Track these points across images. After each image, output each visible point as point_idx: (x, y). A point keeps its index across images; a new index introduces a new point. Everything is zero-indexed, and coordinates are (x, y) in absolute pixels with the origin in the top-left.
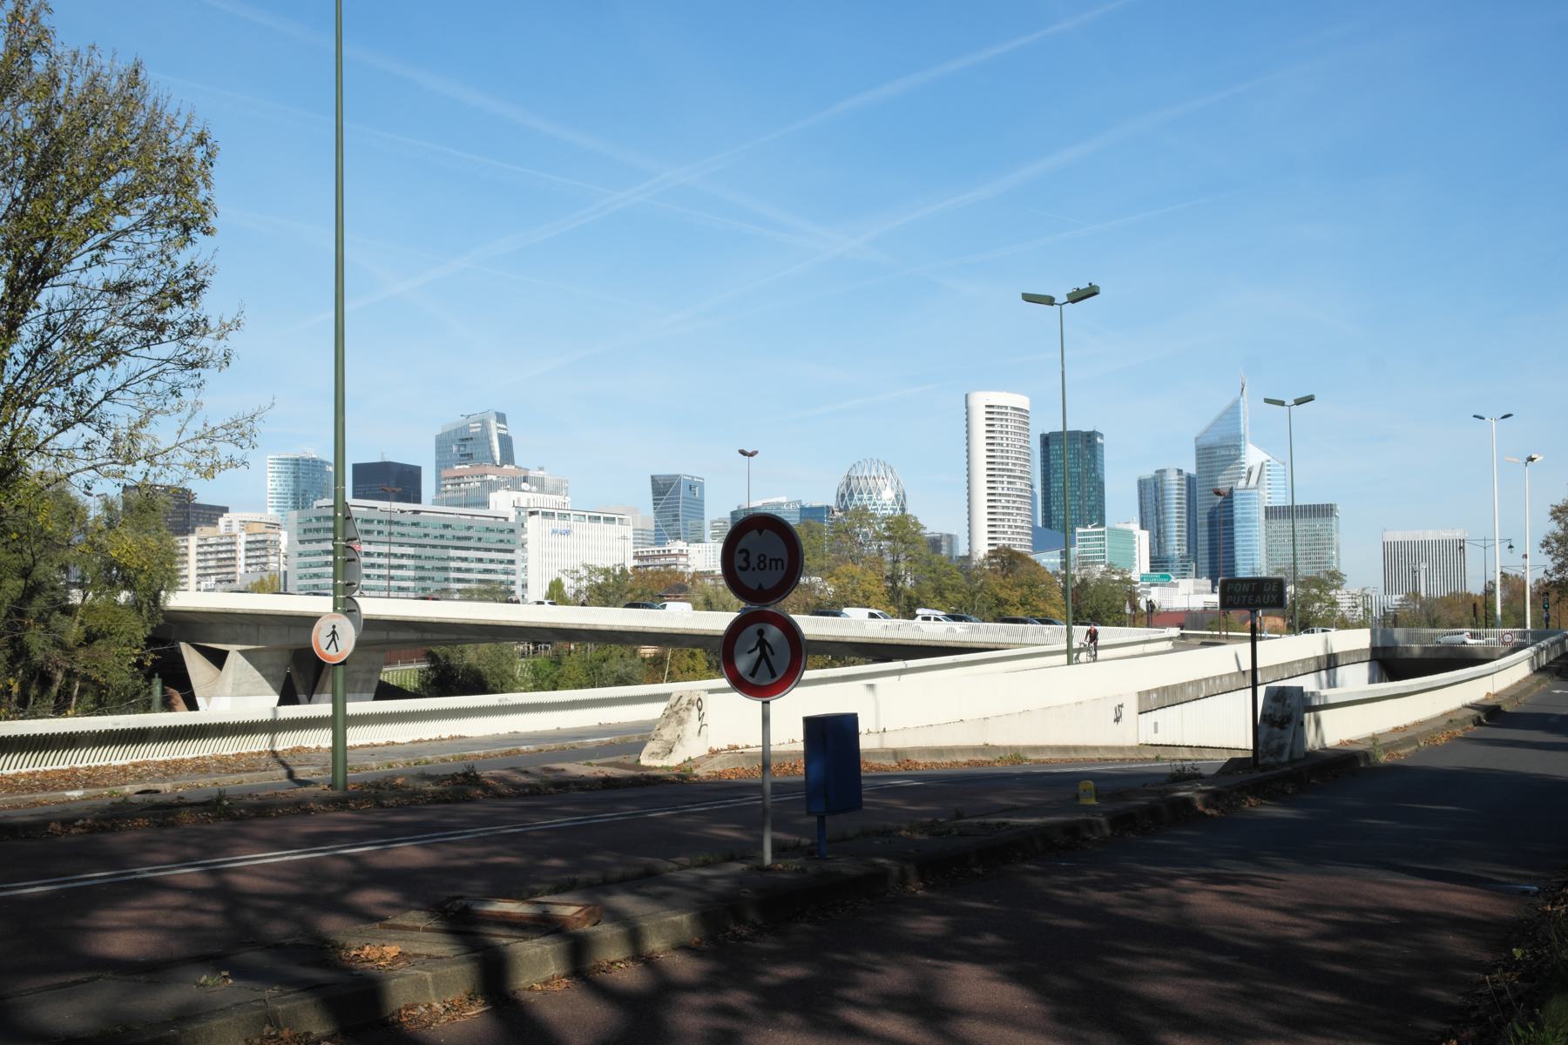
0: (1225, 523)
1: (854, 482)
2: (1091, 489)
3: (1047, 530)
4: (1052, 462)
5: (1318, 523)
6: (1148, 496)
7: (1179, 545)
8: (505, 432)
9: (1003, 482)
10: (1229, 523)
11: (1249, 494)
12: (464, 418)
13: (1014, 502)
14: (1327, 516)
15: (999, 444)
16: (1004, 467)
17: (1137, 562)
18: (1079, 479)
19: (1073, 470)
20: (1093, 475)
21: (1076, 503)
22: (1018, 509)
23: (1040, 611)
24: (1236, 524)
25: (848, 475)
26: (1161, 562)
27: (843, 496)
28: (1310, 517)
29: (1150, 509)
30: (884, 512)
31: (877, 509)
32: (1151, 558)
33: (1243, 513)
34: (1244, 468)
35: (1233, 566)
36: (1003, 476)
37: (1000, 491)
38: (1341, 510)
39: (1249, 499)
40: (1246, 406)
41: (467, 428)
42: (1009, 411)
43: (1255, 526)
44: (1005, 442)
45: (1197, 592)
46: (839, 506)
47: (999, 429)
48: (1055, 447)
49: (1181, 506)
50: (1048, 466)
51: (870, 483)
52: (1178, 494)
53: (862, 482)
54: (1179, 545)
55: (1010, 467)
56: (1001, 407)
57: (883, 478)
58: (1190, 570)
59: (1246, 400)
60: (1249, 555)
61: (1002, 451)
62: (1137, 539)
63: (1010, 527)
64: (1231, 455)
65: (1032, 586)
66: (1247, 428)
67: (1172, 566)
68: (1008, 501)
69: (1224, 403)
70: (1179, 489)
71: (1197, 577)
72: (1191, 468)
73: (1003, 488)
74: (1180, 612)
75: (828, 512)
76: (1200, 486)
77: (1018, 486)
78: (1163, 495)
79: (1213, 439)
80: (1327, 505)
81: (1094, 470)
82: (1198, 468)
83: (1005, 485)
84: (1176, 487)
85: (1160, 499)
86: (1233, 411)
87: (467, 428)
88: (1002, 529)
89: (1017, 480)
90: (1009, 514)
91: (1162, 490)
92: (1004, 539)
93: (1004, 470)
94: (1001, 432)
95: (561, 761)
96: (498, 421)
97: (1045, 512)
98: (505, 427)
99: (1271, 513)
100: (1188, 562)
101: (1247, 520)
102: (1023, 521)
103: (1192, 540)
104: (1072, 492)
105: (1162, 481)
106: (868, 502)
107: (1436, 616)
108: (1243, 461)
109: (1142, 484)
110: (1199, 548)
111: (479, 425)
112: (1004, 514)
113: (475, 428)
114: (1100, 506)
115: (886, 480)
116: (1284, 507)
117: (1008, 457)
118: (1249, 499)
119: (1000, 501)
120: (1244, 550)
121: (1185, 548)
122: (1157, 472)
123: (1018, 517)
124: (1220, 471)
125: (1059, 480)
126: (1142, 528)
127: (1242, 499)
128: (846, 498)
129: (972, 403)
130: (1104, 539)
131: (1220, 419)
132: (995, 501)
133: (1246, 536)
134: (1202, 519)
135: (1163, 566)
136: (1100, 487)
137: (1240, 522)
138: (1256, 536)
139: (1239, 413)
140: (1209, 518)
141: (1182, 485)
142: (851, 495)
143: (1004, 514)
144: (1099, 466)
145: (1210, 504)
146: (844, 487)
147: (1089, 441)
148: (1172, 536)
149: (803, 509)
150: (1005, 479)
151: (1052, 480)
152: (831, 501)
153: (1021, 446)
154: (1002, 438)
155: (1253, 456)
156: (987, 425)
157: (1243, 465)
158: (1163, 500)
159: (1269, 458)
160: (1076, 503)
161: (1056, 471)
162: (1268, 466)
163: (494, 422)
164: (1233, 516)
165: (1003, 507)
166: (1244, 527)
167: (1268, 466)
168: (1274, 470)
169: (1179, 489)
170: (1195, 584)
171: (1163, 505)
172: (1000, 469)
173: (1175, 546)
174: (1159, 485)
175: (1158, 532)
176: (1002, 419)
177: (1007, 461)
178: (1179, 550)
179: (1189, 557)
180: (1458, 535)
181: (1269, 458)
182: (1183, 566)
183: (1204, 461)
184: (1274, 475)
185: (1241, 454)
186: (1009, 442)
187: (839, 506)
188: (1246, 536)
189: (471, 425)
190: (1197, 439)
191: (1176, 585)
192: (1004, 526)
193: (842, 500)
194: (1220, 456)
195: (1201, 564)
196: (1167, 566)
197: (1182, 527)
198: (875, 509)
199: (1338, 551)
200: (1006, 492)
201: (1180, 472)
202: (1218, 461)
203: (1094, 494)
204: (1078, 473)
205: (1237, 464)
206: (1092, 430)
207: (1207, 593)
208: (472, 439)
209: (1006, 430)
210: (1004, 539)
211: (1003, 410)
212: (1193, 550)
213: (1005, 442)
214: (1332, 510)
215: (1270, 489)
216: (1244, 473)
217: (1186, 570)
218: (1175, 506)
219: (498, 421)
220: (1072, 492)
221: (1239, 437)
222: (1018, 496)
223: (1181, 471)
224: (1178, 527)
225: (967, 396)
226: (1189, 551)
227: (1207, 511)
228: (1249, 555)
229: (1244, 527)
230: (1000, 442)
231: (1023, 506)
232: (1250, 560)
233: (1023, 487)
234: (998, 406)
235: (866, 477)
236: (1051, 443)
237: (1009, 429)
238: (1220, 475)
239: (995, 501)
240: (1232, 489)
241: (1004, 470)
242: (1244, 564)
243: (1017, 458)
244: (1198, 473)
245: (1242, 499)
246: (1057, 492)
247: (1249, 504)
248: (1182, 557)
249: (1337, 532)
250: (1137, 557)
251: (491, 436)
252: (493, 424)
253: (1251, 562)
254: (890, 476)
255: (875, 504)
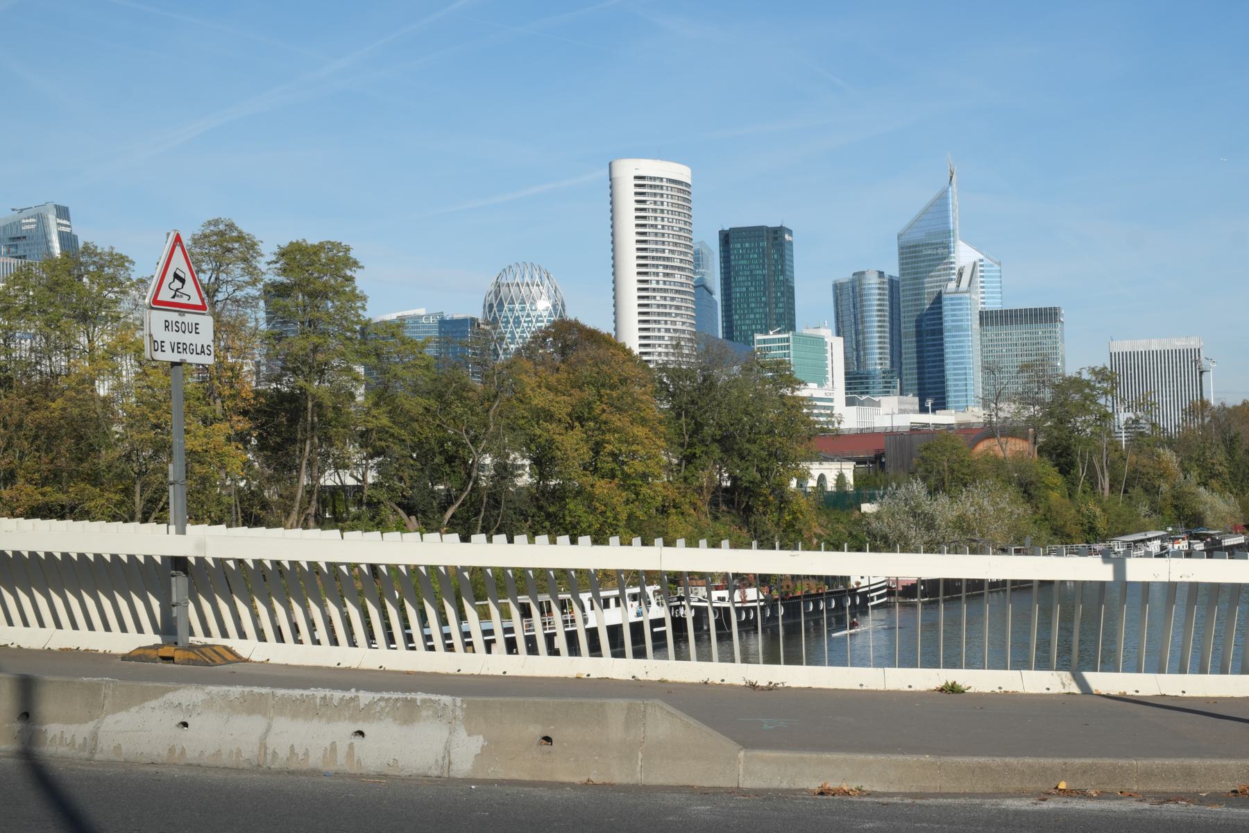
0: (933, 332)
1: (504, 290)
2: (779, 294)
3: (728, 342)
4: (733, 263)
5: (1040, 330)
6: (845, 318)
7: (881, 359)
8: (68, 230)
9: (657, 274)
10: (938, 332)
11: (961, 299)
12: (16, 212)
13: (673, 299)
14: (1051, 321)
15: (652, 225)
16: (659, 255)
17: (829, 376)
18: (764, 282)
19: (758, 272)
20: (781, 278)
21: (761, 310)
22: (677, 307)
23: (615, 431)
24: (946, 334)
25: (497, 283)
26: (861, 378)
27: (491, 306)
28: (1031, 323)
29: (848, 319)
30: (539, 324)
31: (531, 321)
32: (846, 374)
33: (953, 321)
34: (953, 268)
35: (943, 382)
36: (657, 266)
37: (654, 285)
38: (1065, 316)
39: (960, 304)
40: (956, 198)
41: (18, 224)
42: (664, 184)
43: (968, 336)
44: (659, 222)
45: (902, 411)
46: (486, 318)
47: (653, 206)
48: (736, 246)
49: (883, 329)
50: (729, 267)
51: (522, 290)
52: (879, 300)
53: (514, 290)
54: (881, 359)
55: (667, 254)
56: (655, 179)
57: (538, 285)
58: (894, 387)
59: (955, 190)
60: (961, 369)
61: (656, 234)
62: (829, 348)
63: (667, 330)
64: (937, 254)
65: (600, 384)
66: (957, 222)
67: (874, 383)
68: (665, 298)
69: (929, 196)
70: (880, 294)
71: (901, 394)
72: (893, 270)
73: (658, 282)
74: (879, 433)
75: (472, 325)
76: (904, 307)
77: (677, 279)
78: (862, 301)
79: (917, 236)
80: (1050, 309)
81: (783, 272)
82: (902, 269)
83: (661, 278)
84: (877, 291)
85: (858, 305)
86: (941, 203)
87: (18, 224)
88: (656, 334)
89: (677, 272)
90: (666, 314)
91: (861, 296)
92: (660, 346)
93: (658, 258)
94: (655, 210)
95: (156, 622)
96: (58, 216)
97: (726, 322)
98: (68, 223)
99: (987, 318)
100: (892, 377)
101: (959, 328)
102: (683, 323)
103: (896, 322)
104: (756, 297)
105: (861, 284)
106: (520, 313)
107: (1232, 434)
108: (953, 260)
109: (838, 289)
110: (904, 362)
111: (34, 220)
112: (659, 314)
113: (29, 225)
114: (790, 313)
115: (541, 287)
116: (1001, 311)
117: (663, 243)
118: (960, 304)
119: (655, 297)
120: (954, 364)
121: (888, 362)
122: (854, 274)
123: (678, 319)
124: (925, 272)
125: (742, 284)
126: (838, 334)
127: (952, 305)
128: (495, 309)
129: (616, 174)
130: (788, 347)
131: (925, 211)
132: (647, 297)
133: (957, 347)
134: (908, 327)
135: (862, 383)
136: (789, 293)
137: (949, 331)
138: (969, 346)
139: (947, 204)
140: (917, 326)
141: (883, 289)
142: (501, 304)
143: (659, 314)
144: (787, 268)
145: (917, 310)
146: (492, 295)
147: (776, 239)
148: (872, 348)
149: (443, 323)
150: (661, 270)
151: (733, 285)
152: (478, 313)
153: (681, 229)
154: (656, 218)
155: (964, 255)
156: (637, 201)
157: (953, 266)
158: (862, 306)
159: (982, 257)
160: (761, 310)
161: (737, 274)
162: (981, 266)
163: (54, 217)
164: (942, 324)
165: (658, 306)
166: (956, 336)
167: (981, 266)
168: (988, 271)
169: (880, 294)
170: (900, 403)
171: (862, 312)
172: (653, 258)
173: (877, 360)
174: (857, 289)
175: (857, 342)
176: (655, 195)
177: (663, 247)
178: (881, 364)
179: (892, 372)
180: (1193, 343)
181: (982, 257)
182: (886, 382)
183: (909, 260)
184: (987, 277)
185: (950, 253)
186: (666, 223)
187: (486, 318)
188: (957, 347)
189: (24, 221)
190: (899, 236)
191: (878, 404)
192: (659, 330)
193: (490, 311)
194: (926, 255)
195: (907, 380)
196: (867, 383)
197: (884, 337)
198: (528, 322)
199: (1063, 362)
200: (661, 286)
201: (881, 274)
202: (922, 261)
203: (782, 299)
204: (764, 276)
205: (946, 264)
206: (779, 225)
207: (914, 412)
208: (24, 237)
209: (662, 208)
210: (660, 346)
211: (657, 183)
212: (897, 364)
213: (659, 222)
214: (1056, 314)
215: (984, 293)
216: (954, 274)
217: (889, 387)
218: (876, 329)
219: (58, 216)
220: (756, 297)
221: (948, 233)
222: (677, 292)
223: (883, 273)
224: (880, 337)
225: (610, 164)
226: (892, 366)
227: (914, 319)
228: (961, 369)
229: (956, 336)
230: (653, 222)
231: (683, 304)
232: (962, 374)
233: (684, 280)
234: (651, 178)
235: (527, 283)
236: (731, 240)
237: (665, 207)
238: (925, 278)
239: (647, 297)
240: (940, 292)
241: (658, 258)
242: (955, 380)
243: (676, 244)
244: (902, 275)
245: (952, 305)
246: (740, 298)
247: (961, 310)
248: (884, 372)
249: (1063, 341)
250: (829, 369)
251: (50, 234)
252: (52, 220)
253: (964, 377)
254: (546, 282)
255: (528, 316)
